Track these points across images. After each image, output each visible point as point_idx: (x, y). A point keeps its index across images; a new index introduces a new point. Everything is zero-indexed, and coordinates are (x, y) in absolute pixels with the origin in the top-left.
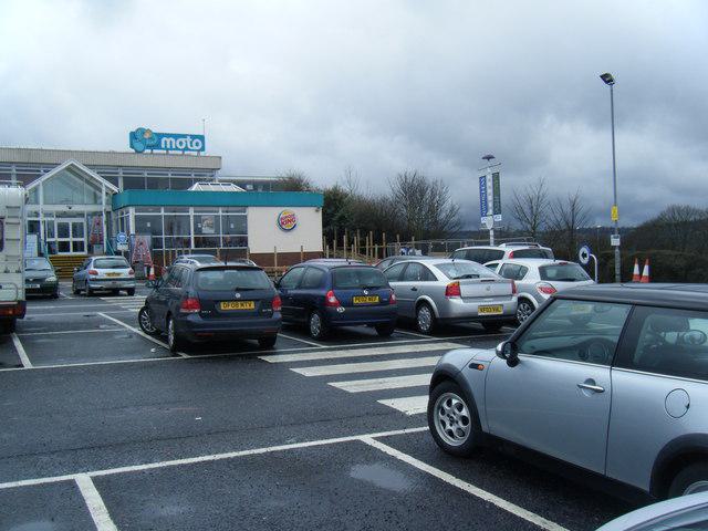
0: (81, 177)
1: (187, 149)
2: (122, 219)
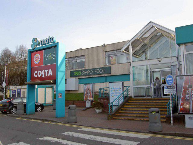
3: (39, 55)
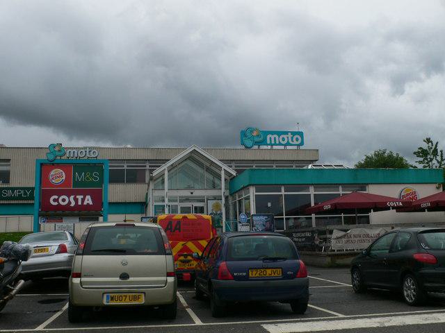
0: (201, 165)
1: (288, 144)
2: (240, 201)
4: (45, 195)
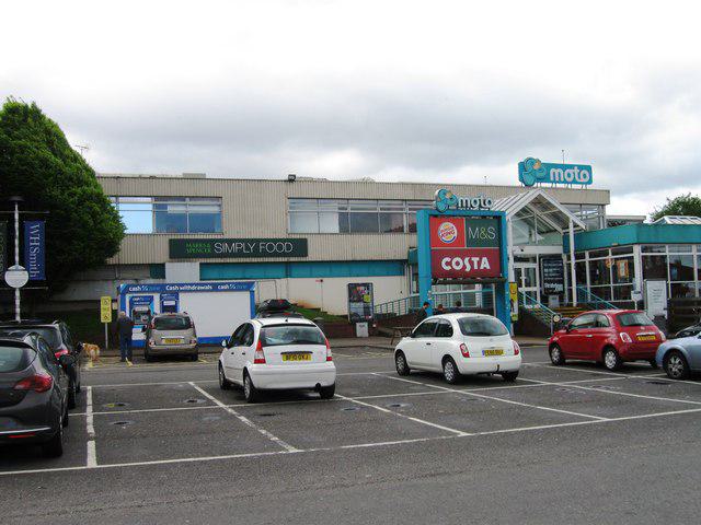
1: (574, 182)
3: (451, 225)
4: (436, 257)
